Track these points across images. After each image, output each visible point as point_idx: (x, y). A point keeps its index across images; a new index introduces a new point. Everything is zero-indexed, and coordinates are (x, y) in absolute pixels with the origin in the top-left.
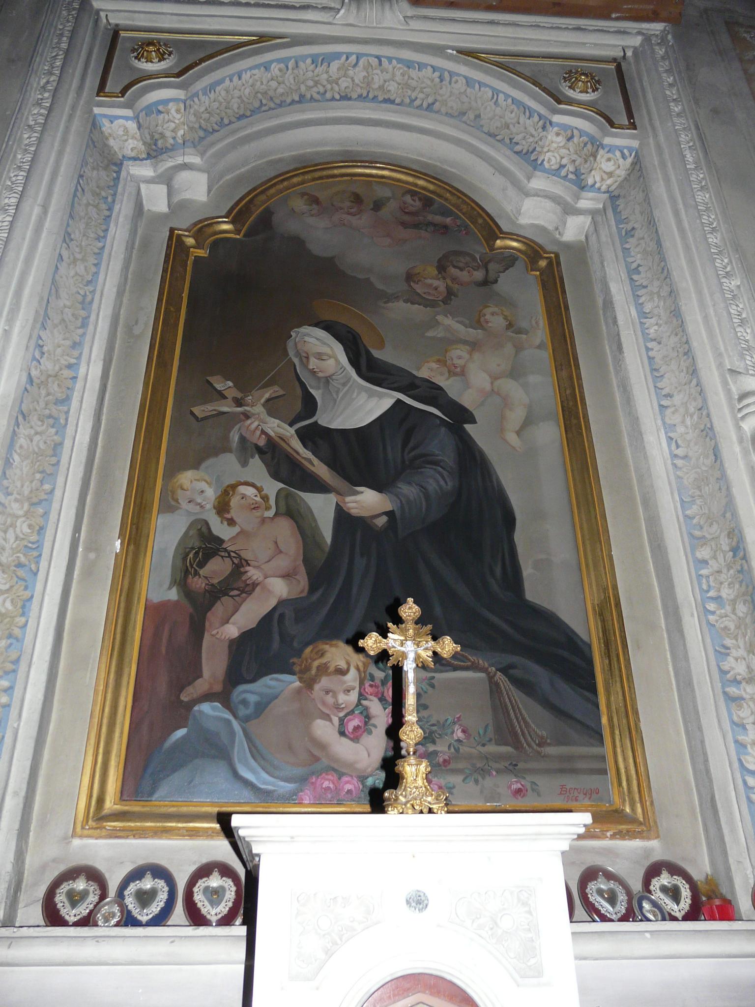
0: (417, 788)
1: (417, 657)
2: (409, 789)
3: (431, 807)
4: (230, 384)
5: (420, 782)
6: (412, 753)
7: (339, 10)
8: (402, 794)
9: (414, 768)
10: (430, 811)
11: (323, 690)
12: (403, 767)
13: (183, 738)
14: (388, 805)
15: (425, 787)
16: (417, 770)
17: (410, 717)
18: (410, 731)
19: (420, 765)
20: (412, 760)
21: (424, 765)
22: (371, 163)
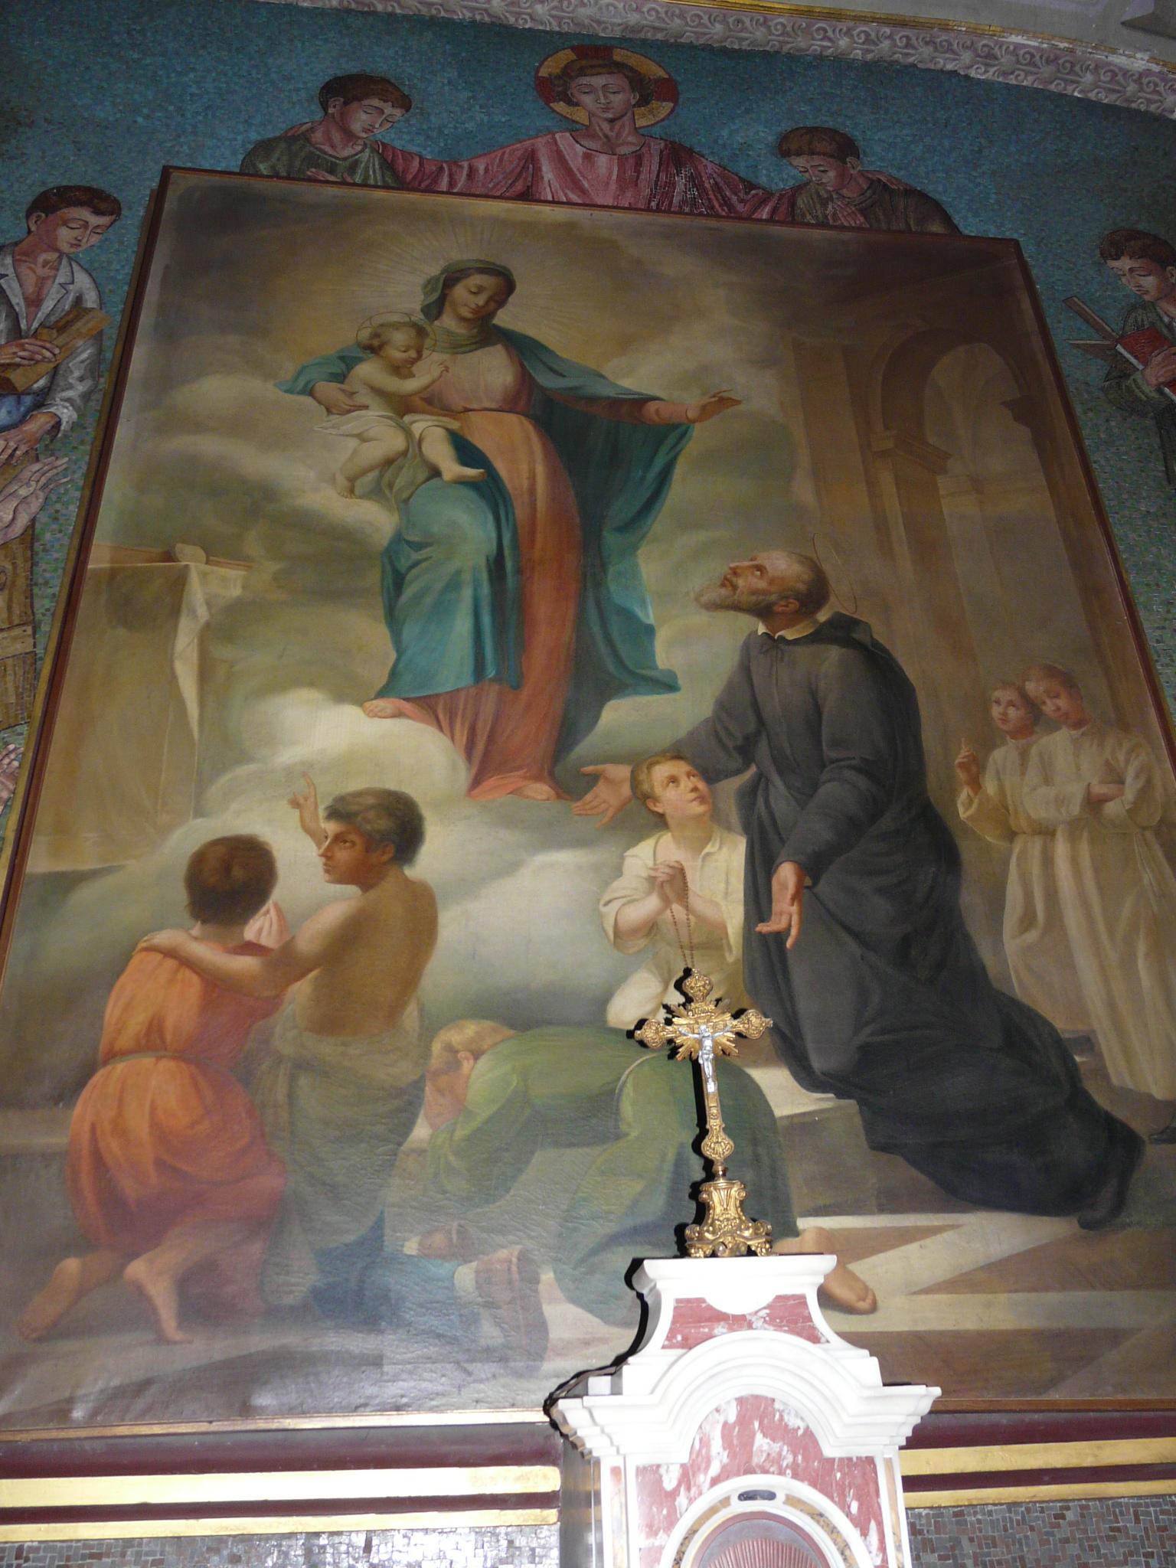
0: (728, 1220)
1: (716, 1044)
2: (717, 1223)
3: (749, 1243)
4: (1105, 101)
5: (732, 1212)
6: (721, 1173)
7: (41, 325)
8: (708, 1231)
9: (723, 1193)
10: (751, 1253)
11: (668, 785)
12: (710, 1194)
13: (786, 627)
14: (691, 1246)
15: (740, 1218)
16: (729, 1196)
17: (714, 1123)
18: (715, 1143)
19: (731, 1188)
20: (721, 1183)
21: (735, 1189)
22: (1121, 1498)
